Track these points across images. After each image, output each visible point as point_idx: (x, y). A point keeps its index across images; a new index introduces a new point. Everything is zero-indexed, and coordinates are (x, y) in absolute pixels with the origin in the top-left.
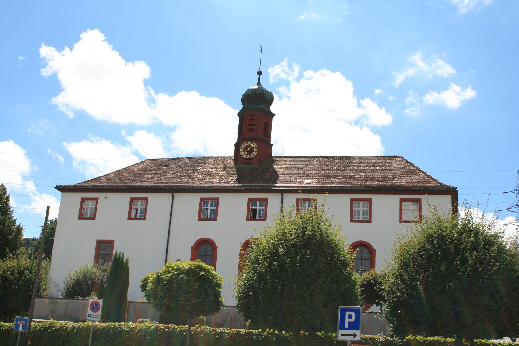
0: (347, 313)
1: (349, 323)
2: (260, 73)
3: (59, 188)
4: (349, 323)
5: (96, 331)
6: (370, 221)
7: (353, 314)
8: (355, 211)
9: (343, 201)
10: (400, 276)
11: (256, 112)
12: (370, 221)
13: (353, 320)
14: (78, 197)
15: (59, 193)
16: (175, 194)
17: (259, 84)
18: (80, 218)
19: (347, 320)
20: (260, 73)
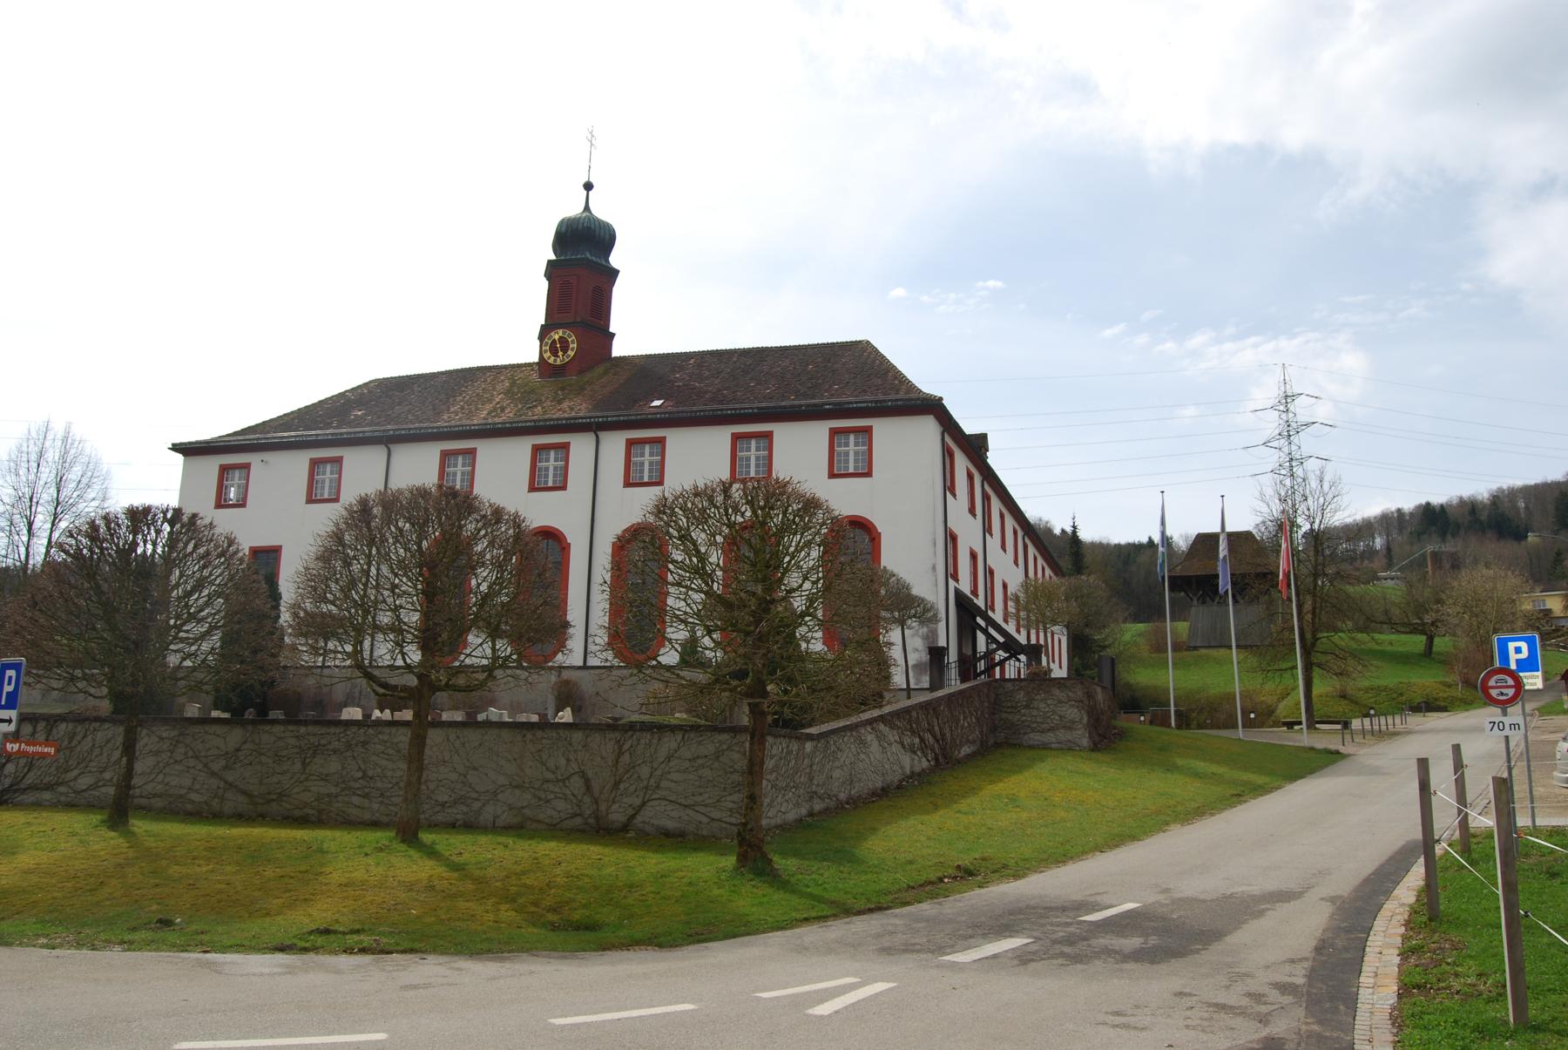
0: (1512, 646)
1: (1518, 661)
2: (588, 186)
3: (177, 448)
4: (1518, 661)
5: (961, 692)
6: (869, 474)
7: (1524, 645)
8: (839, 454)
9: (518, 452)
10: (732, 625)
11: (582, 263)
12: (869, 474)
13: (1525, 654)
14: (212, 465)
15: (179, 458)
16: (602, 435)
17: (587, 208)
18: (310, 500)
19: (1513, 657)
20: (588, 186)
